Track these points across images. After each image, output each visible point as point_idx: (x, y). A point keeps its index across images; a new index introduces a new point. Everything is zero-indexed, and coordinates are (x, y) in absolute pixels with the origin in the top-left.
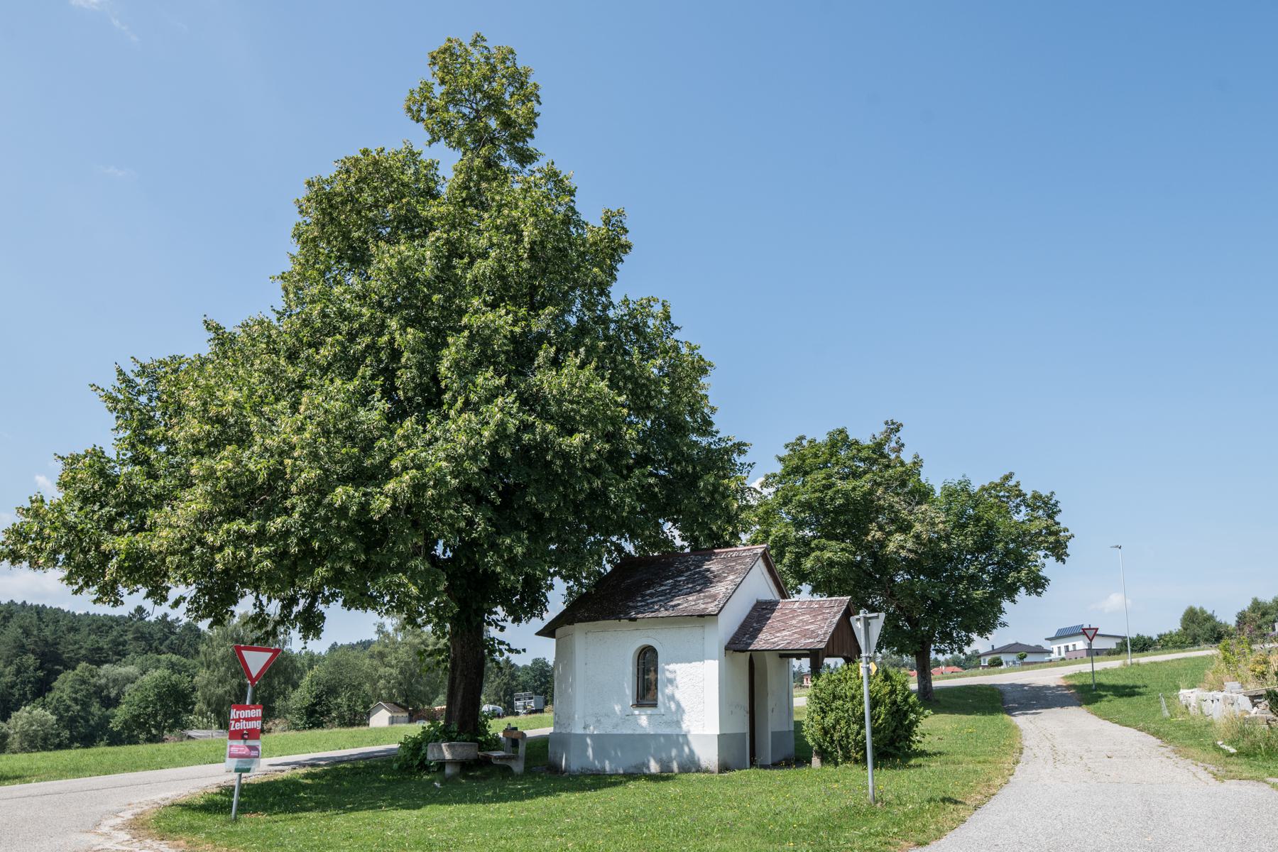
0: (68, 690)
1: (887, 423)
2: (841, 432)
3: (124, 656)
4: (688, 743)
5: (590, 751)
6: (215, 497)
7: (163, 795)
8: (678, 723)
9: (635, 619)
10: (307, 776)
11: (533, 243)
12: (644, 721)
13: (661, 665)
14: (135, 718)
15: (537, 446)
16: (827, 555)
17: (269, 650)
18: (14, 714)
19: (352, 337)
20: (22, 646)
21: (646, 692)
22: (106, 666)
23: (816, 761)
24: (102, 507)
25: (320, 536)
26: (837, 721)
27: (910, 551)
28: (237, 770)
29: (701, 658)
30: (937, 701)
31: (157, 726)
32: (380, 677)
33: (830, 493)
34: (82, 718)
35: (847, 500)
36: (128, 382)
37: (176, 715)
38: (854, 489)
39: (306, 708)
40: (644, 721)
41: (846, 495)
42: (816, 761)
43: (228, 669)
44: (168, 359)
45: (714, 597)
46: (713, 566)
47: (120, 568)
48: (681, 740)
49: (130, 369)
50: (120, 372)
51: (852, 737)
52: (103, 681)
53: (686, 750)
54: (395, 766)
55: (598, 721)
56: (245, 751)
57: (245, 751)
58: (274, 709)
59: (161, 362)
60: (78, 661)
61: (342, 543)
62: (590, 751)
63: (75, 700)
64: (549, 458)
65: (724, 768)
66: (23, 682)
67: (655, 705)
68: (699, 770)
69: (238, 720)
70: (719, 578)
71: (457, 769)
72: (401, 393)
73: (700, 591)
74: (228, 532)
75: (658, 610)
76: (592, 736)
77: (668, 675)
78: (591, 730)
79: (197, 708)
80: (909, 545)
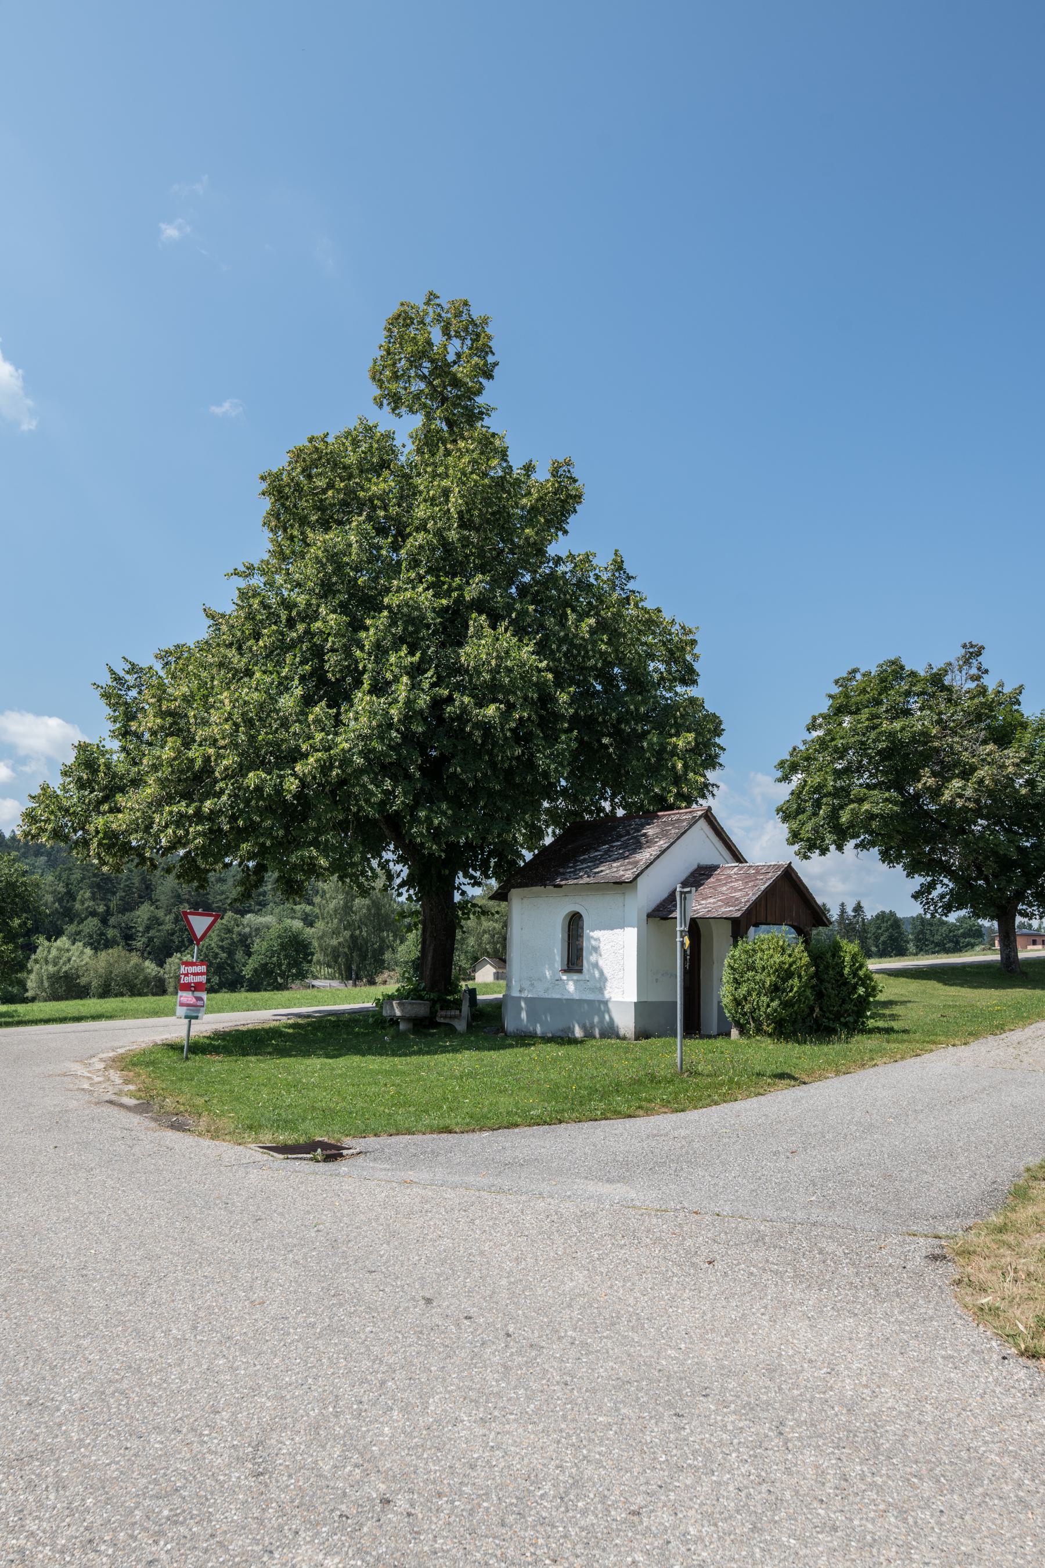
0: (216, 939)
1: (964, 646)
2: (893, 663)
3: (265, 905)
4: (608, 1011)
5: (524, 1015)
6: (162, 783)
7: (164, 1037)
8: (601, 990)
9: (560, 886)
10: (291, 1026)
11: (460, 513)
12: (571, 987)
13: (587, 931)
14: (264, 966)
15: (459, 718)
16: (866, 806)
17: (211, 915)
18: (169, 960)
19: (291, 623)
20: (179, 896)
21: (574, 959)
22: (249, 916)
23: (735, 1032)
24: (91, 792)
25: (245, 815)
26: (749, 993)
27: (969, 799)
28: (186, 1017)
29: (622, 926)
30: (1025, 974)
31: (282, 975)
32: (485, 932)
33: (873, 735)
34: (229, 965)
35: (893, 742)
36: (117, 679)
37: (296, 964)
38: (903, 729)
39: (413, 962)
40: (571, 987)
41: (891, 735)
42: (735, 1032)
43: (341, 921)
44: (172, 648)
45: (636, 863)
46: (650, 831)
47: (100, 844)
48: (601, 1006)
49: (120, 668)
50: (112, 672)
51: (763, 1009)
52: (247, 930)
53: (607, 1017)
54: (371, 1020)
55: (532, 985)
56: (193, 1001)
57: (193, 1001)
58: (383, 961)
59: (166, 652)
60: (225, 911)
61: (262, 821)
62: (524, 1015)
63: (222, 948)
64: (468, 729)
65: (642, 1034)
66: (181, 930)
67: (580, 971)
68: (618, 1037)
69: (186, 975)
70: (650, 842)
71: (410, 1026)
72: (330, 675)
73: (625, 858)
74: (171, 813)
75: (581, 877)
76: (526, 999)
77: (593, 943)
78: (525, 994)
79: (315, 958)
80: (969, 793)
